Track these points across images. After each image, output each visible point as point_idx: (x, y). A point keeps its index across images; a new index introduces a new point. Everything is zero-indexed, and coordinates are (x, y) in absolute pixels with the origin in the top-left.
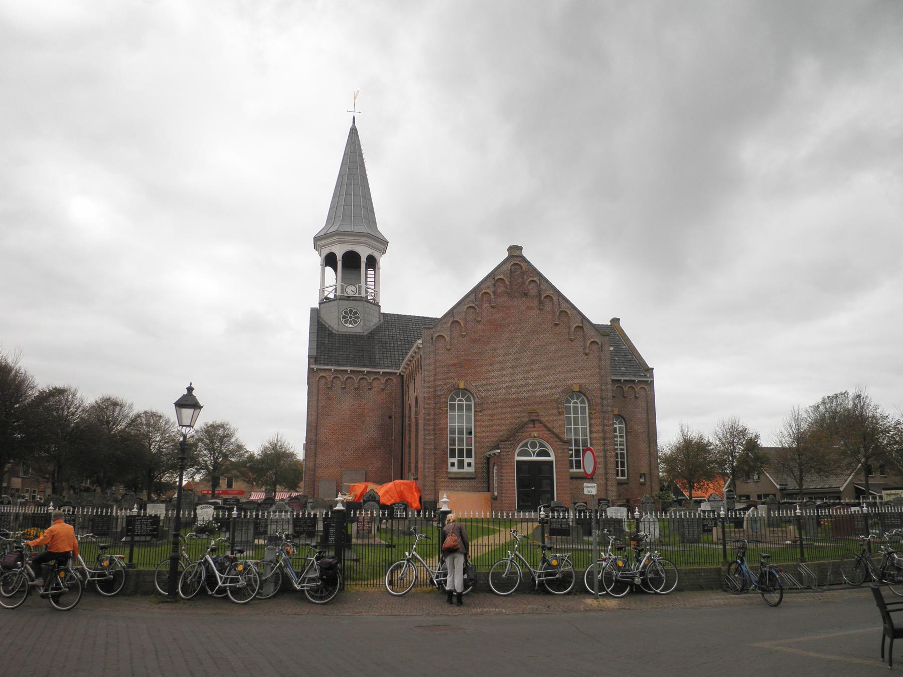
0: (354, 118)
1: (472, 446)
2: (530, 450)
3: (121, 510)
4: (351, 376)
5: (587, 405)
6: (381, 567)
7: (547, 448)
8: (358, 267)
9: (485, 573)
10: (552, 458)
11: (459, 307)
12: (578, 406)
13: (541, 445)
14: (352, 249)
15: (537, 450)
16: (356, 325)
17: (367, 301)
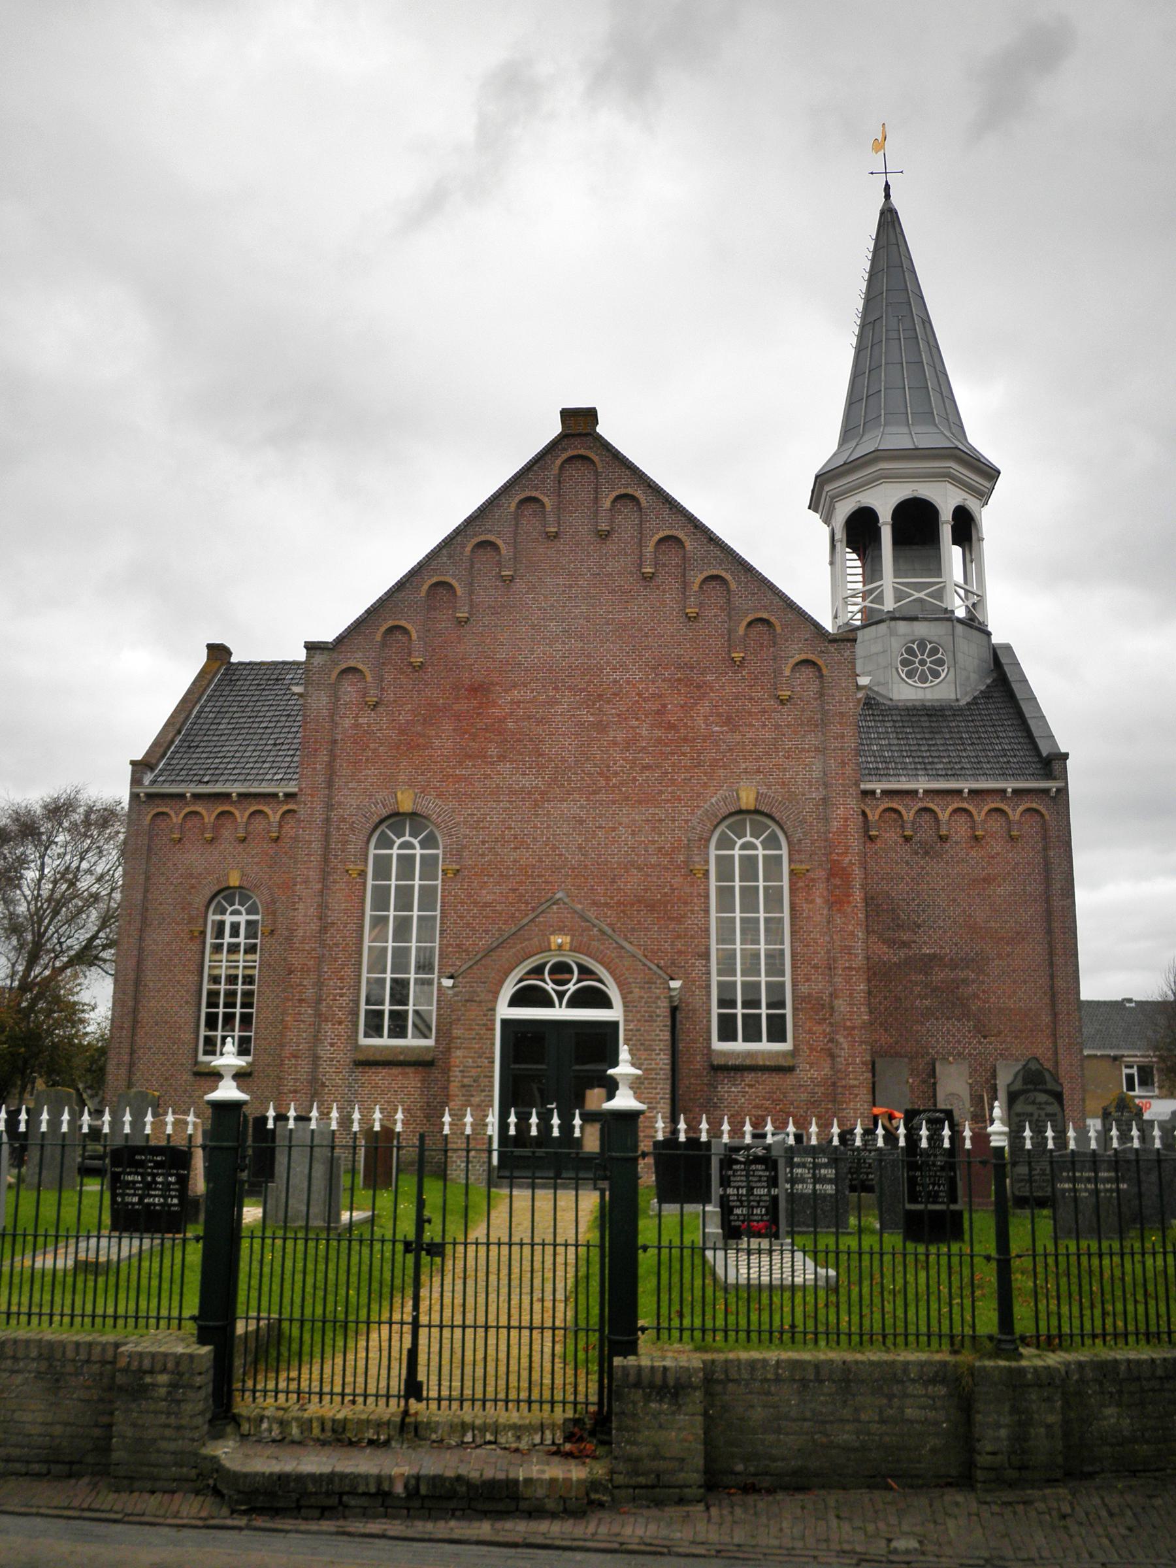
0: (887, 187)
1: (783, 976)
2: (550, 987)
3: (693, 1142)
4: (931, 805)
5: (784, 852)
6: (308, 1326)
7: (601, 981)
8: (932, 539)
9: (183, 1355)
10: (255, 987)
11: (400, 596)
12: (414, 856)
13: (585, 971)
14: (916, 494)
15: (572, 987)
16: (903, 676)
17: (947, 616)
